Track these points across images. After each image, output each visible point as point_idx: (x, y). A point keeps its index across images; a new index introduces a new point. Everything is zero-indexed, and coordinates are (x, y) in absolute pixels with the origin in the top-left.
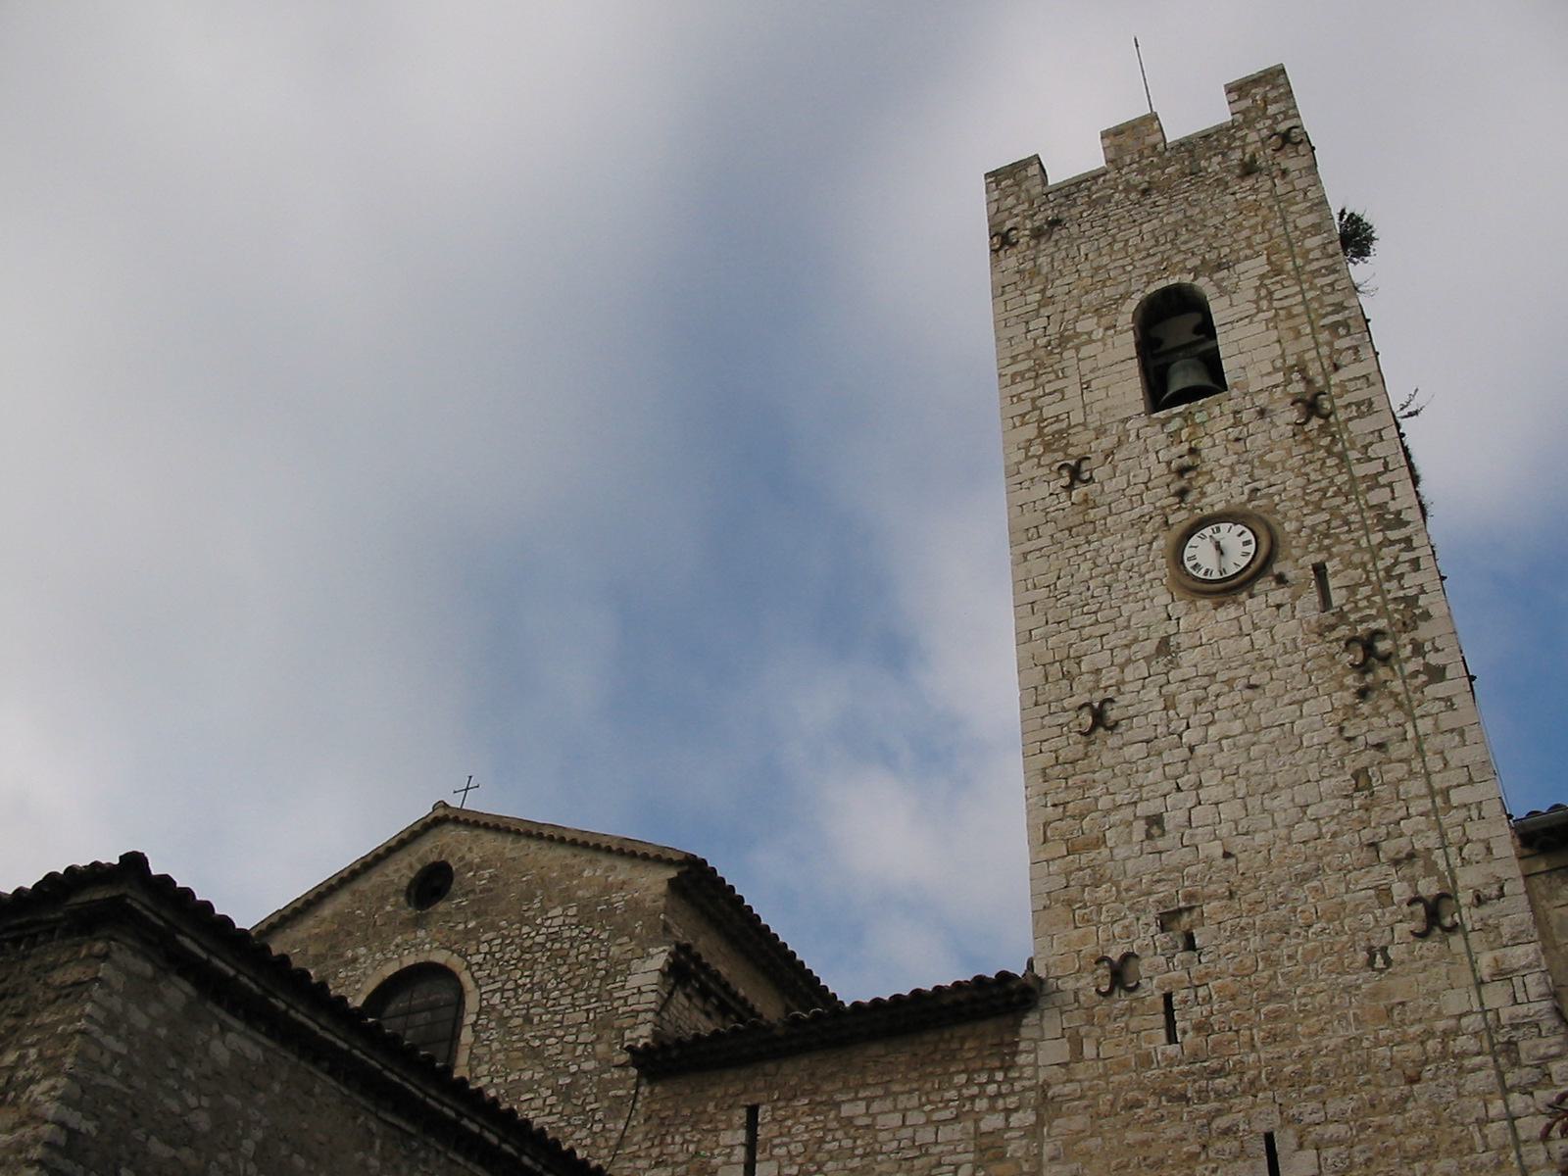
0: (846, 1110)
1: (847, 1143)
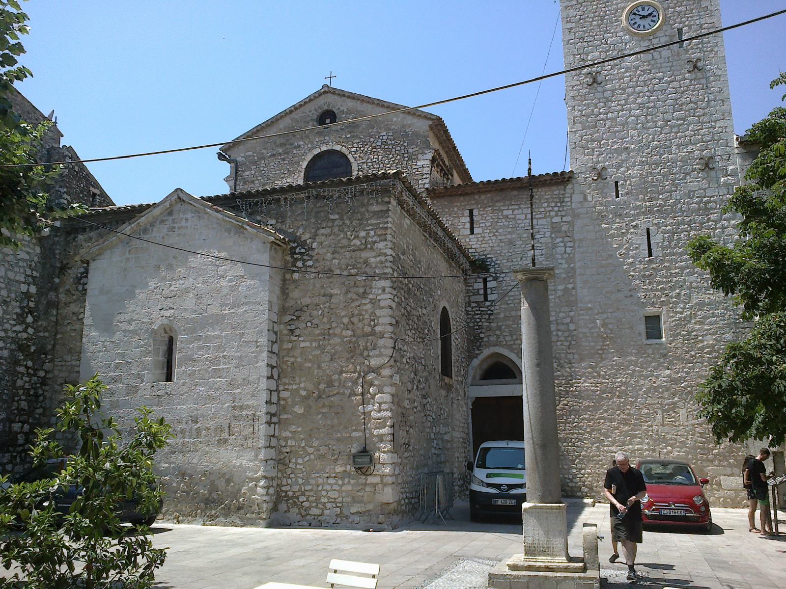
0: (505, 213)
1: (507, 223)
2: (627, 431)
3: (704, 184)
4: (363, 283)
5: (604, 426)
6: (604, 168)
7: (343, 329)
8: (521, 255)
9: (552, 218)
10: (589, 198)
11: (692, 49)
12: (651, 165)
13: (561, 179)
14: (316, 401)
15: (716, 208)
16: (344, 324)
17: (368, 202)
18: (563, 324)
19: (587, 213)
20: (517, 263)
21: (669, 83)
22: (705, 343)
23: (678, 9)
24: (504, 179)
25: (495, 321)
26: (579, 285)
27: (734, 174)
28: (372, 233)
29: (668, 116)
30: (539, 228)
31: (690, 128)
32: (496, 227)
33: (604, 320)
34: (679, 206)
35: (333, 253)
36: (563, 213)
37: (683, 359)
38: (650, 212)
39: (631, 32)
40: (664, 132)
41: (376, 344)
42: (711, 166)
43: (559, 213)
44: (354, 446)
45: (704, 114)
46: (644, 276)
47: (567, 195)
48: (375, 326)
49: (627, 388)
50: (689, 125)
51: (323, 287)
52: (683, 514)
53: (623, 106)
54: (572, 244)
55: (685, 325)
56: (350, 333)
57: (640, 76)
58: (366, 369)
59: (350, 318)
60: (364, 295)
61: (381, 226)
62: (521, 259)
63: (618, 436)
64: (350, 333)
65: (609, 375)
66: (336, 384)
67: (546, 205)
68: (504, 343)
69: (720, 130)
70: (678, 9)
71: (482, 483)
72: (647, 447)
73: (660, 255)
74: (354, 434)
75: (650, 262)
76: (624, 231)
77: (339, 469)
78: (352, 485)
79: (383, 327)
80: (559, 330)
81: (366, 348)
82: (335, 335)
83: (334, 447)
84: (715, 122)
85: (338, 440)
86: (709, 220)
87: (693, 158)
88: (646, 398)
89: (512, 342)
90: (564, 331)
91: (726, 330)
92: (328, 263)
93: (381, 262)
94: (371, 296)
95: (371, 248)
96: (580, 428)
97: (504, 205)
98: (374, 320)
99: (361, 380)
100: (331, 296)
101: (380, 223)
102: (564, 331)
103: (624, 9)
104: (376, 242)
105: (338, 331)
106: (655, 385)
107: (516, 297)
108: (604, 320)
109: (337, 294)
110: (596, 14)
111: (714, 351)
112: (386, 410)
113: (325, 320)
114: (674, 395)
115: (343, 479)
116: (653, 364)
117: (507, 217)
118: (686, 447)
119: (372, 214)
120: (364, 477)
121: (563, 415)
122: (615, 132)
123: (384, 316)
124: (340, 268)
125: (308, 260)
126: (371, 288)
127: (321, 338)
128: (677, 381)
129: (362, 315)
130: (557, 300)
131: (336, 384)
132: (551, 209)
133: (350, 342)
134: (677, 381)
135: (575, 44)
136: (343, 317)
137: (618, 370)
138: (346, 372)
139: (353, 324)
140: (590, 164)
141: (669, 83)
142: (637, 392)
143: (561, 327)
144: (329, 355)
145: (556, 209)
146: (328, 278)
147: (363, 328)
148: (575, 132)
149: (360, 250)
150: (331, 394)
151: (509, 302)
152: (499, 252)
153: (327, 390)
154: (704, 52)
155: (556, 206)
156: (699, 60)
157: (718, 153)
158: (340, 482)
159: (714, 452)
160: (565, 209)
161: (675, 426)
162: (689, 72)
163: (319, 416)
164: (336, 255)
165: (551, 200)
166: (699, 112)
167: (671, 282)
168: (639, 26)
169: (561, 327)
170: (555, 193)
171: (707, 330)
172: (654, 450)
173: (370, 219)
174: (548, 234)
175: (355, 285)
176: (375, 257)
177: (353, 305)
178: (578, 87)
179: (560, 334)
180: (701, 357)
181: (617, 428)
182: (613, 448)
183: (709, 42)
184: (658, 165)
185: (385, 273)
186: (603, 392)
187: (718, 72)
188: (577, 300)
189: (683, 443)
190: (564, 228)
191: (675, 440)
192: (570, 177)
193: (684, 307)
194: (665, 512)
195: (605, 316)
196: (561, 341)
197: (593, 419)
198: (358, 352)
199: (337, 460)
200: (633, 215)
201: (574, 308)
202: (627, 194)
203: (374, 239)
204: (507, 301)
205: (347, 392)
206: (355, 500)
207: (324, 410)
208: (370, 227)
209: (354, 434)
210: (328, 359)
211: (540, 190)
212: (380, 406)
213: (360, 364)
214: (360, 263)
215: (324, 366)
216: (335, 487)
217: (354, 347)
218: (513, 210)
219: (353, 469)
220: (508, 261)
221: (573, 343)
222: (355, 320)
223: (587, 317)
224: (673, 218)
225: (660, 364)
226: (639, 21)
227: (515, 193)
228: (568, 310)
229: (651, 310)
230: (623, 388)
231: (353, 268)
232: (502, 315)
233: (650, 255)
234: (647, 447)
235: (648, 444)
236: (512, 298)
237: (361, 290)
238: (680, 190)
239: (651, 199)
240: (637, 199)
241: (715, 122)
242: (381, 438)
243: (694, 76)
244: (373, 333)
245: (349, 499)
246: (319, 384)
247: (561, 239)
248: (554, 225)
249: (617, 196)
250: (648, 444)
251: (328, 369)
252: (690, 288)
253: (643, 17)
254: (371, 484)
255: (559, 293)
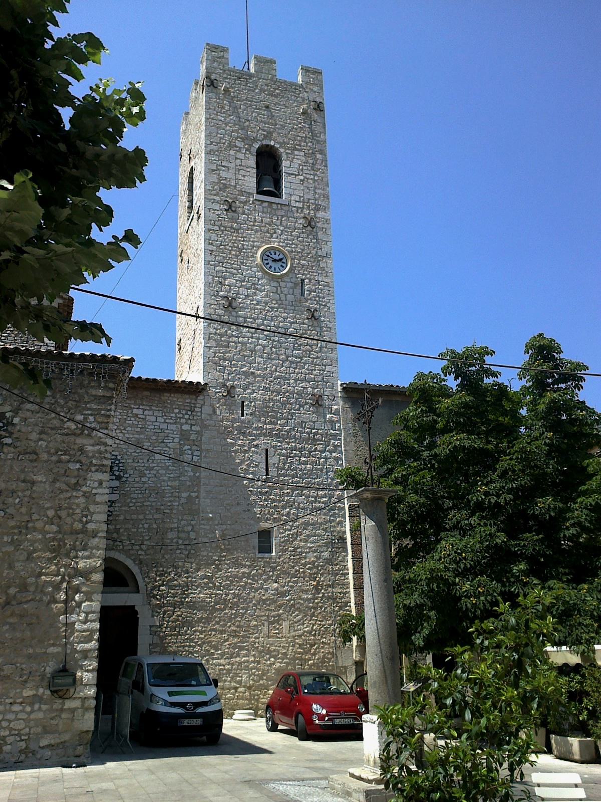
0: (135, 411)
1: (136, 423)
2: (236, 643)
3: (314, 417)
4: (76, 473)
5: (215, 638)
6: (233, 387)
7: (46, 523)
8: (148, 457)
9: (182, 424)
10: (218, 412)
11: (311, 299)
12: (272, 392)
13: (193, 389)
14: (3, 608)
15: (322, 441)
16: (48, 517)
17: (89, 383)
18: (184, 532)
19: (215, 426)
20: (143, 465)
21: (292, 323)
22: (308, 560)
23: (302, 262)
24: (140, 378)
25: (113, 522)
26: (203, 494)
27: (337, 413)
28: (91, 418)
29: (289, 352)
30: (169, 433)
31: (306, 367)
32: (125, 425)
33: (223, 531)
34: (293, 433)
35: (40, 433)
36: (193, 422)
37: (289, 573)
38: (269, 434)
39: (264, 270)
40: (285, 365)
41: (86, 545)
42: (320, 403)
43: (189, 422)
44: (50, 664)
45: (317, 357)
46: (261, 493)
47: (198, 405)
48: (87, 522)
49: (239, 600)
50: (305, 364)
51: (23, 471)
52: (352, 722)
53: (252, 334)
54: (199, 453)
55: (292, 541)
56: (55, 528)
57: (268, 311)
58: (72, 572)
59: (56, 511)
60: (76, 486)
61: (103, 412)
62: (148, 461)
63: (228, 648)
64: (55, 528)
65: (224, 587)
66: (32, 589)
67: (177, 411)
68: (121, 547)
69: (329, 374)
70: (302, 262)
71: (167, 703)
72: (253, 659)
73: (276, 475)
74: (52, 650)
75: (266, 481)
76: (246, 448)
77: (27, 693)
78: (45, 712)
79: (98, 524)
80: (179, 538)
81: (74, 548)
82: (35, 529)
83: (24, 666)
84: (325, 366)
85: (30, 656)
86: (316, 450)
87: (307, 393)
88: (255, 610)
89: (130, 547)
90: (184, 540)
91: (324, 549)
92: (33, 444)
93: (100, 452)
94: (84, 489)
95: (89, 435)
96: (192, 640)
97: (136, 404)
98: (86, 516)
99: (65, 585)
100: (33, 483)
101: (102, 409)
102: (184, 540)
103: (259, 247)
104: (94, 429)
105: (39, 525)
106: (264, 598)
107: (139, 500)
108: (223, 531)
109: (41, 482)
110: (235, 245)
111: (314, 567)
112: (94, 621)
113: (24, 510)
114: (280, 607)
115: (32, 704)
116: (264, 577)
117: (137, 415)
118: (287, 658)
119: (93, 398)
120: (61, 701)
121: (176, 626)
122: (245, 356)
123: (99, 513)
124: (48, 453)
125: (6, 437)
126: (85, 479)
127: (16, 531)
128: (283, 594)
129: (73, 509)
130: (180, 508)
131: (32, 589)
132: (181, 416)
133: (54, 539)
134: (283, 594)
135: (215, 266)
136: (48, 509)
137: (232, 582)
138: (46, 574)
139: (60, 518)
140: (221, 381)
141: (292, 323)
142: (248, 604)
143: (182, 535)
144: (25, 553)
145: (187, 417)
146: (31, 461)
147: (72, 524)
148: (210, 348)
149: (75, 434)
150: (24, 600)
151: (131, 505)
152: (125, 450)
153: (18, 596)
154: (320, 305)
155: (186, 414)
156: (316, 310)
157: (326, 393)
158: (28, 709)
159: (310, 662)
160: (195, 418)
161: (279, 638)
162: (308, 319)
163: (6, 627)
164: (44, 436)
165: (183, 407)
166: (313, 355)
167: (283, 500)
168: (271, 267)
169: (182, 535)
170: (187, 401)
171: (310, 548)
172: (259, 662)
173: (89, 402)
174: (177, 440)
175: (65, 474)
176: (93, 445)
177: (61, 496)
178: (215, 307)
179: (180, 542)
180: (304, 572)
181: (227, 640)
182: (222, 661)
183: (324, 298)
184: (278, 393)
185: (103, 465)
186: (217, 603)
187: (330, 325)
188: (199, 509)
189: (285, 654)
190: (193, 437)
191: (278, 651)
192: (203, 389)
193: (292, 526)
194: (337, 722)
195: (225, 527)
196: (180, 549)
197: (204, 631)
198: (63, 551)
199: (26, 681)
200: (255, 435)
201: (196, 517)
202: (251, 414)
203: (93, 425)
204: (129, 503)
205: (46, 599)
206: (46, 731)
207: (11, 620)
208: (89, 412)
209: (52, 650)
210: (22, 558)
211: (172, 395)
212: (87, 617)
213: (65, 566)
214: (74, 449)
215: (18, 566)
216: (20, 716)
217: (59, 545)
218: (144, 410)
219: (48, 692)
220: (133, 462)
221: (193, 552)
222: (63, 514)
223: (208, 527)
224: (288, 443)
225: (269, 578)
226: (271, 263)
227: (147, 393)
228: (190, 518)
229: (264, 525)
230: (235, 600)
231: (65, 454)
232: (122, 518)
233: (267, 474)
234: (253, 659)
235: (254, 655)
236: (134, 501)
237: (73, 481)
238: (295, 419)
239: (271, 423)
240: (260, 421)
241: (325, 366)
242: (85, 654)
243: (311, 324)
244: (84, 531)
245: (39, 730)
246: (9, 587)
247: (189, 447)
248: (184, 433)
249: (243, 415)
250: (254, 655)
251: (23, 570)
252: (298, 508)
253: (275, 260)
254: (69, 709)
255: (183, 501)
